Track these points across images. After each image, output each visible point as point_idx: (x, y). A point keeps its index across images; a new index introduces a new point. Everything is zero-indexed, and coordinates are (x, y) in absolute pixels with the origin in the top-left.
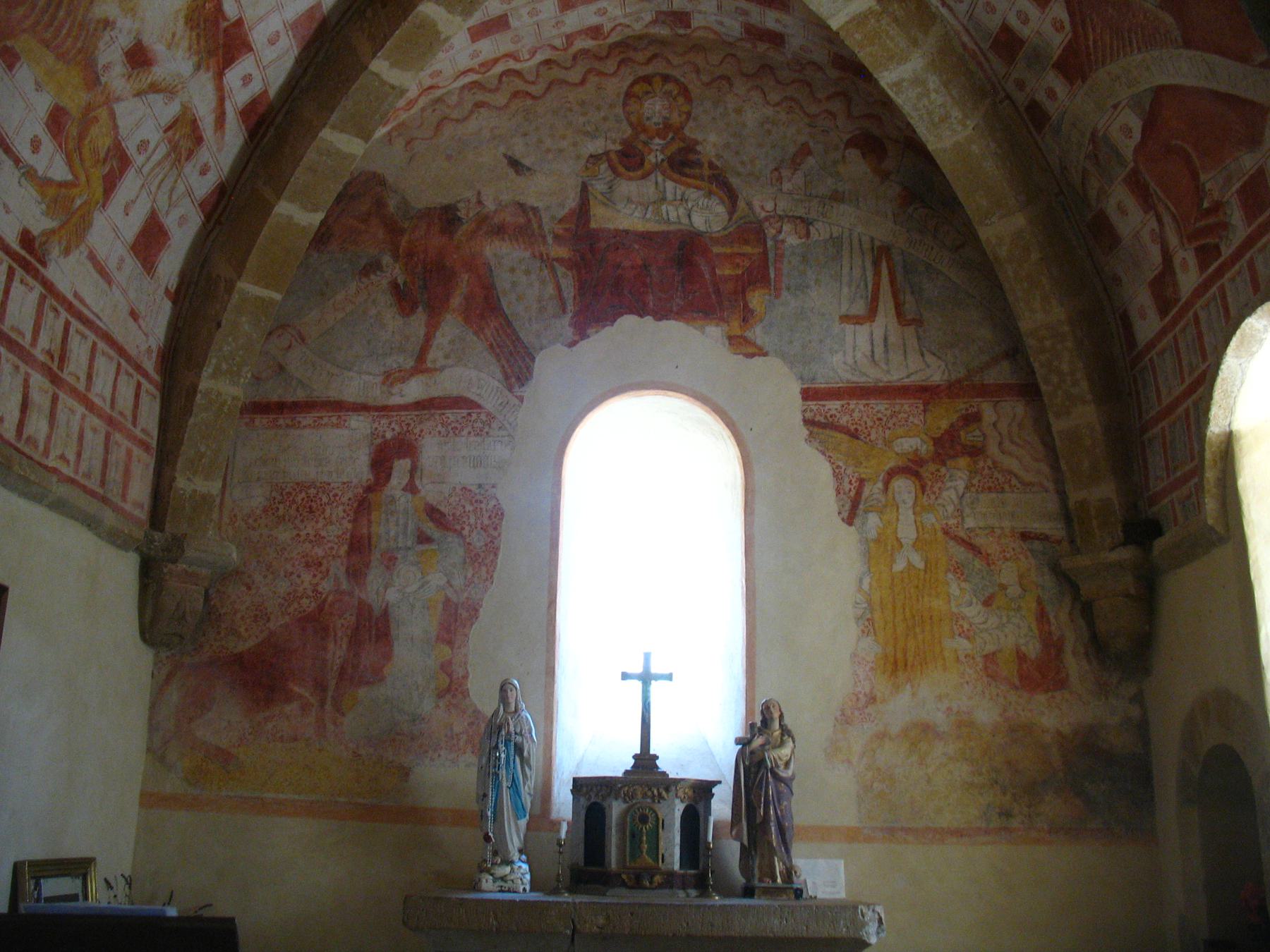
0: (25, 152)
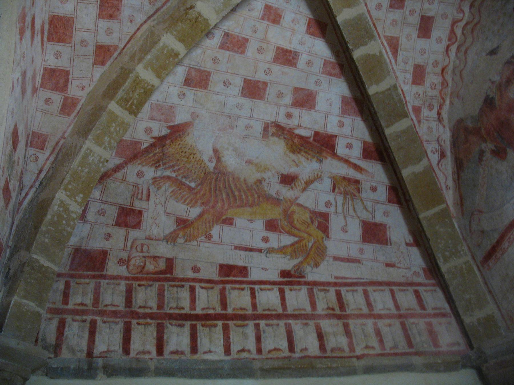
0: (263, 245)
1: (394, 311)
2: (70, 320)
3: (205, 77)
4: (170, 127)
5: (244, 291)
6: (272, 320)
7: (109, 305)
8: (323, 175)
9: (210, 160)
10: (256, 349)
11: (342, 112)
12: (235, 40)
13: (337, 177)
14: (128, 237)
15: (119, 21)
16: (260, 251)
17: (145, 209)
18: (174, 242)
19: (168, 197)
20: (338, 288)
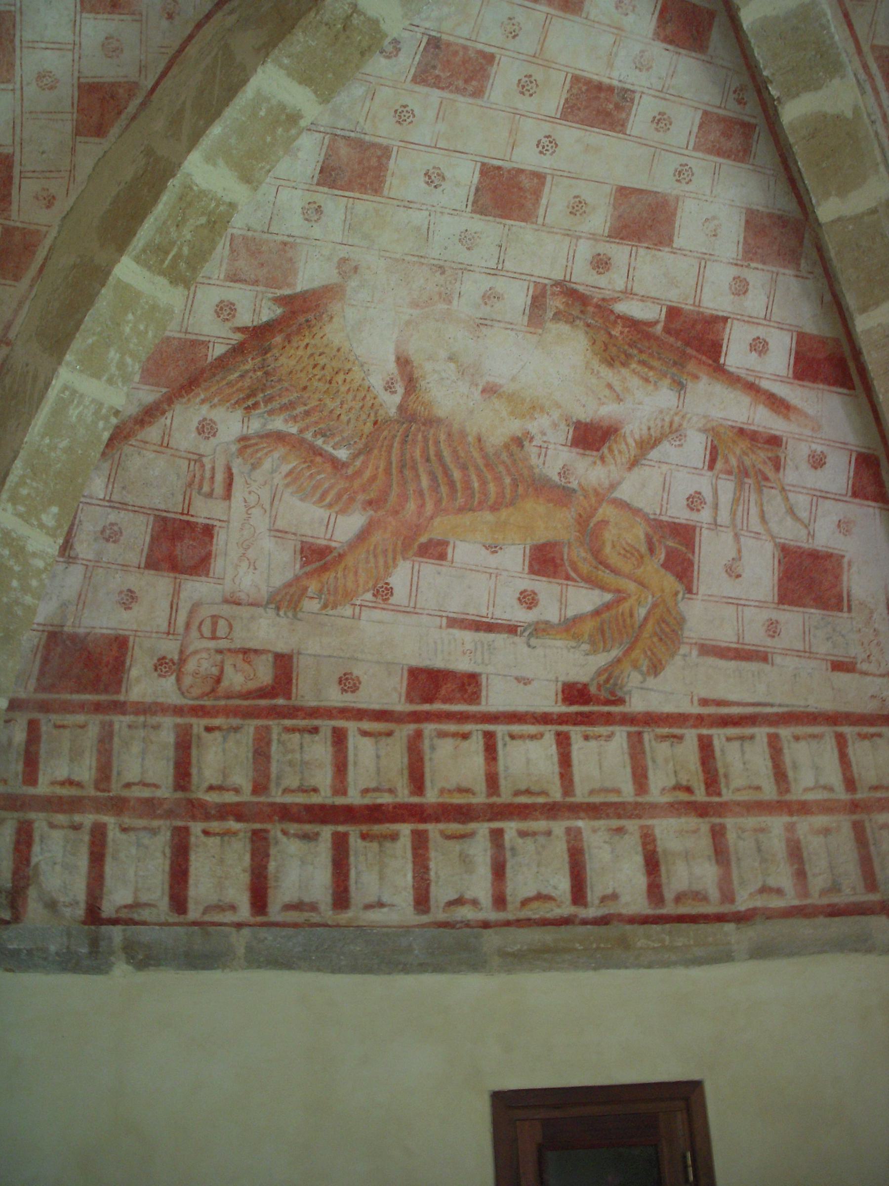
0: (521, 616)
1: (842, 794)
2: (44, 824)
3: (374, 162)
4: (281, 301)
5: (468, 742)
6: (537, 819)
7: (134, 784)
8: (685, 425)
9: (389, 387)
10: (493, 896)
11: (745, 252)
12: (458, 59)
13: (722, 430)
14: (178, 598)
15: (137, 17)
16: (512, 629)
17: (220, 521)
18: (295, 609)
19: (281, 488)
20: (705, 731)
